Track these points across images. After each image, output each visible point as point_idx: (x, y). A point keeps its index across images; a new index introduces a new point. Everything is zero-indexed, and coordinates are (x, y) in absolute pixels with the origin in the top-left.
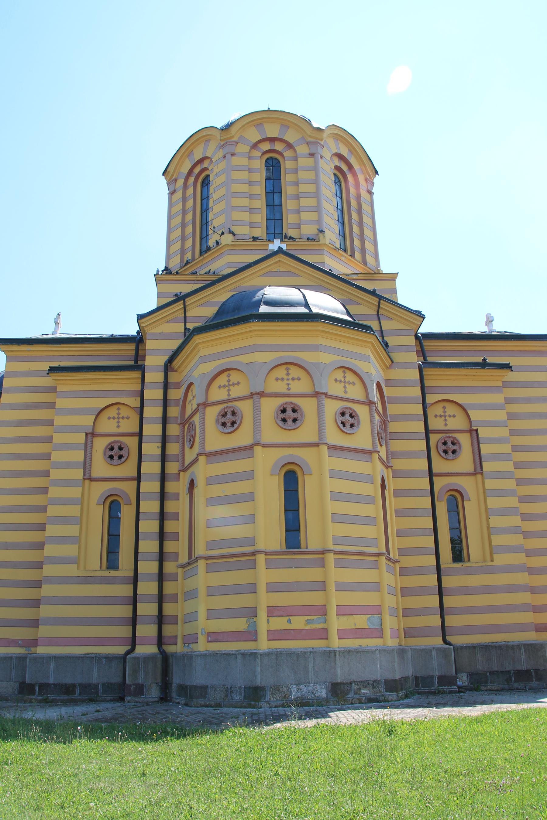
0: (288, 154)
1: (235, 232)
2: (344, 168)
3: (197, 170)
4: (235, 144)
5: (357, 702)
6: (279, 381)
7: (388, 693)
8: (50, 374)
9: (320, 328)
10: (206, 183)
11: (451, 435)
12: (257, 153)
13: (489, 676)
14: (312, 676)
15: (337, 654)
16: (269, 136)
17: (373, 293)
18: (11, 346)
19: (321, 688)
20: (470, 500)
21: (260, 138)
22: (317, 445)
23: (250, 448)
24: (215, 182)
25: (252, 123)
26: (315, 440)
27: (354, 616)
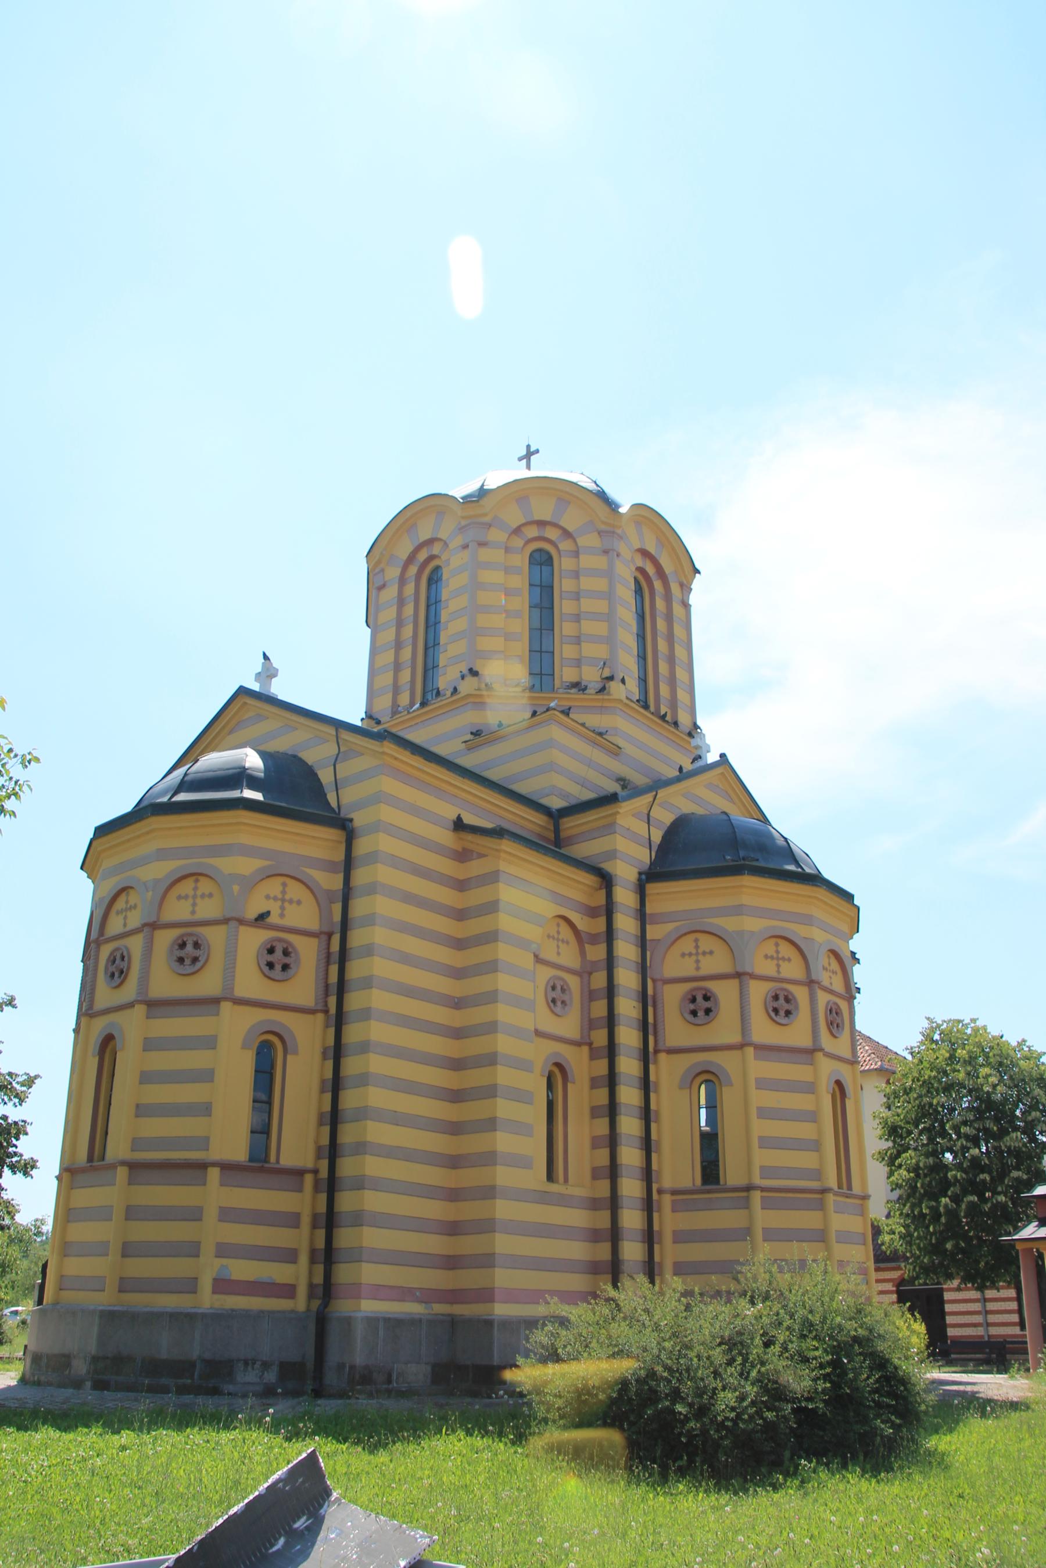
0: (565, 545)
2: (651, 570)
3: (422, 556)
10: (434, 579)
16: (537, 518)
21: (524, 521)
22: (741, 1046)
23: (214, 1002)
24: (452, 583)
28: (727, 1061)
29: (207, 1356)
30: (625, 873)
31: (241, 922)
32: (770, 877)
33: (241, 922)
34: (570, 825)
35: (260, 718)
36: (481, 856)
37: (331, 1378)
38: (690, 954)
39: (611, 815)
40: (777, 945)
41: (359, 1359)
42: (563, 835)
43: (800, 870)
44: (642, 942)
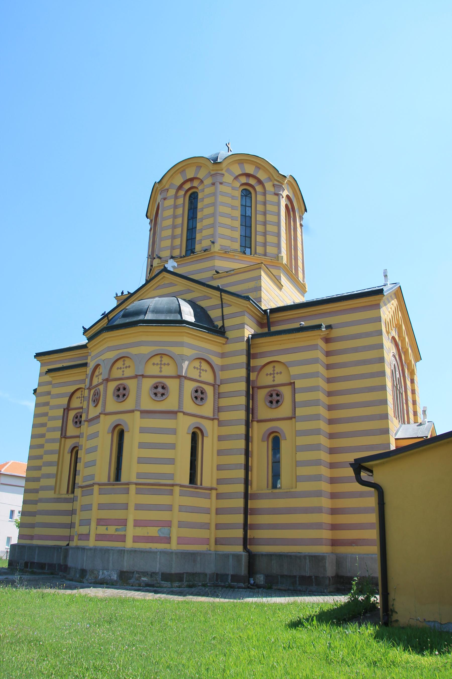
0: (259, 188)
1: (161, 257)
4: (167, 191)
5: (137, 586)
6: (162, 369)
7: (163, 582)
8: (47, 374)
9: (141, 330)
11: (275, 388)
12: (237, 184)
13: (280, 578)
14: (111, 565)
15: (125, 552)
17: (217, 289)
18: (40, 357)
19: (114, 574)
20: (286, 440)
23: (175, 413)
25: (177, 172)
27: (148, 527)
35: (172, 285)
40: (200, 363)
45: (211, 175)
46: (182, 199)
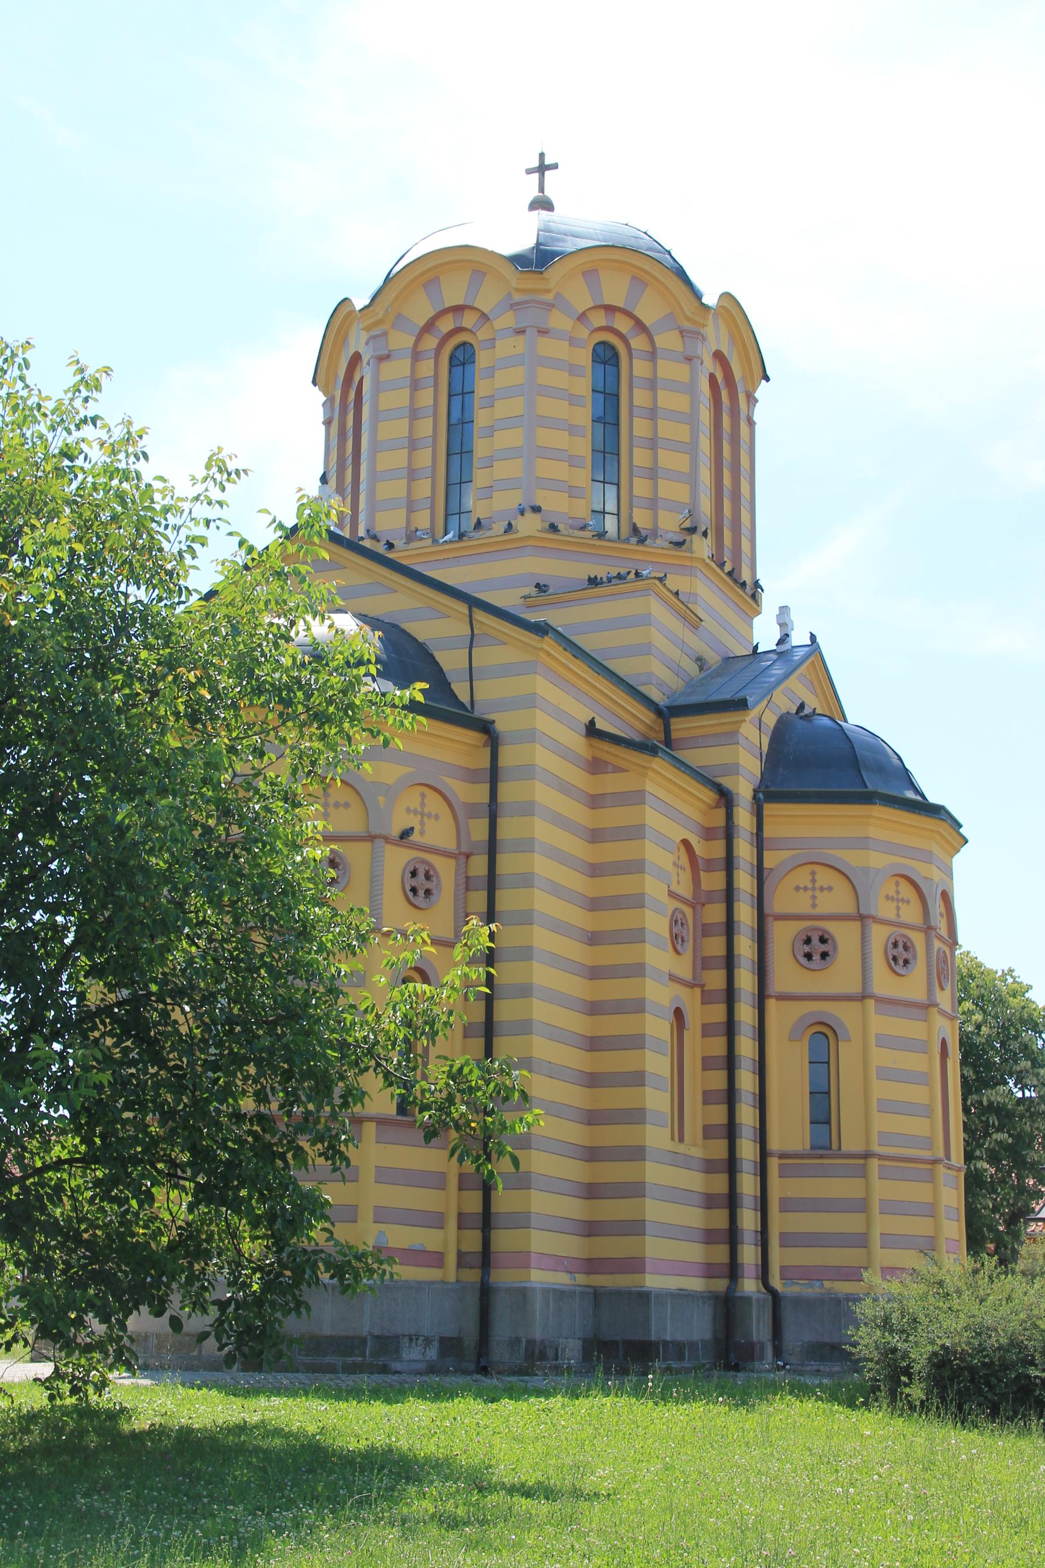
0: (638, 343)
2: (720, 377)
3: (446, 325)
22: (863, 997)
26: (856, 988)
28: (845, 1014)
29: (377, 1332)
30: (744, 789)
31: (387, 839)
32: (506, 621)
33: (387, 839)
34: (680, 726)
36: (619, 770)
37: (499, 1353)
38: (805, 889)
39: (733, 723)
41: (538, 1335)
42: (674, 735)
43: (919, 798)
44: (760, 873)
45: (512, 306)
46: (431, 363)
